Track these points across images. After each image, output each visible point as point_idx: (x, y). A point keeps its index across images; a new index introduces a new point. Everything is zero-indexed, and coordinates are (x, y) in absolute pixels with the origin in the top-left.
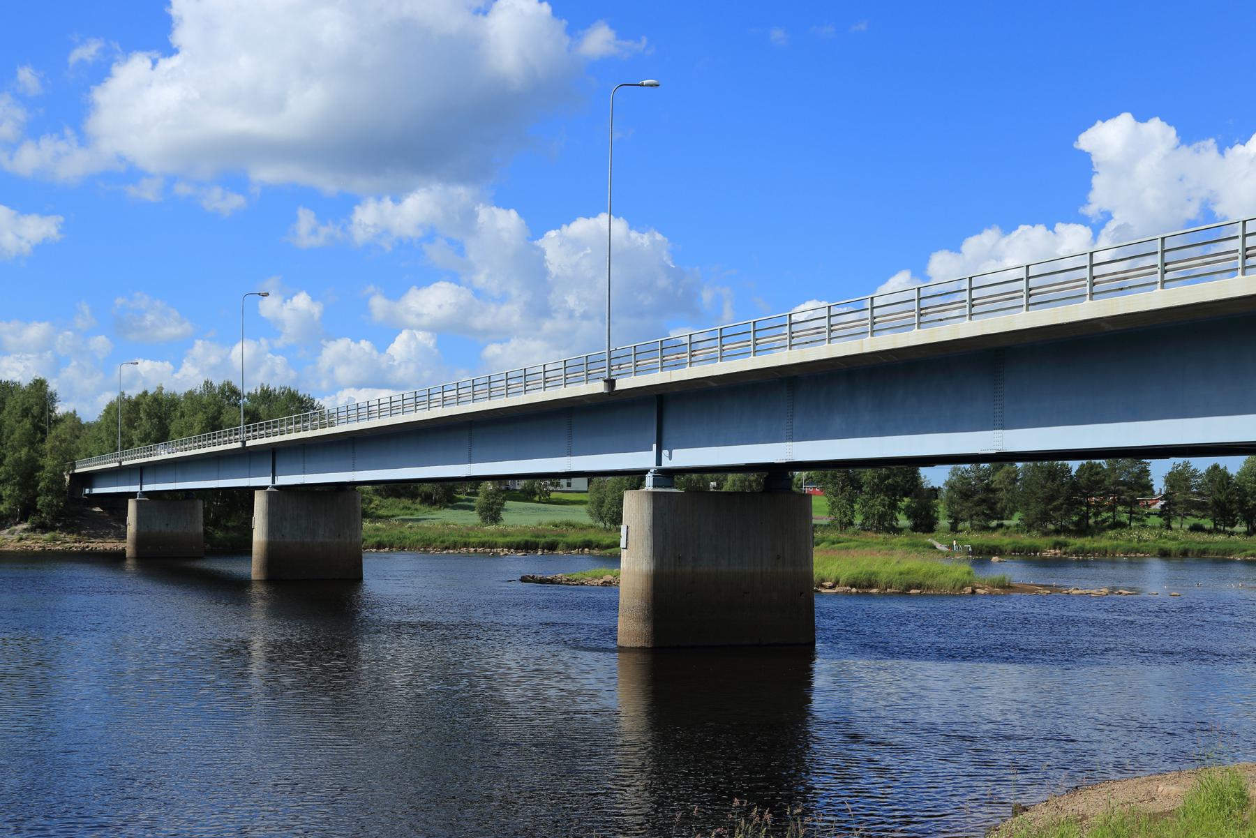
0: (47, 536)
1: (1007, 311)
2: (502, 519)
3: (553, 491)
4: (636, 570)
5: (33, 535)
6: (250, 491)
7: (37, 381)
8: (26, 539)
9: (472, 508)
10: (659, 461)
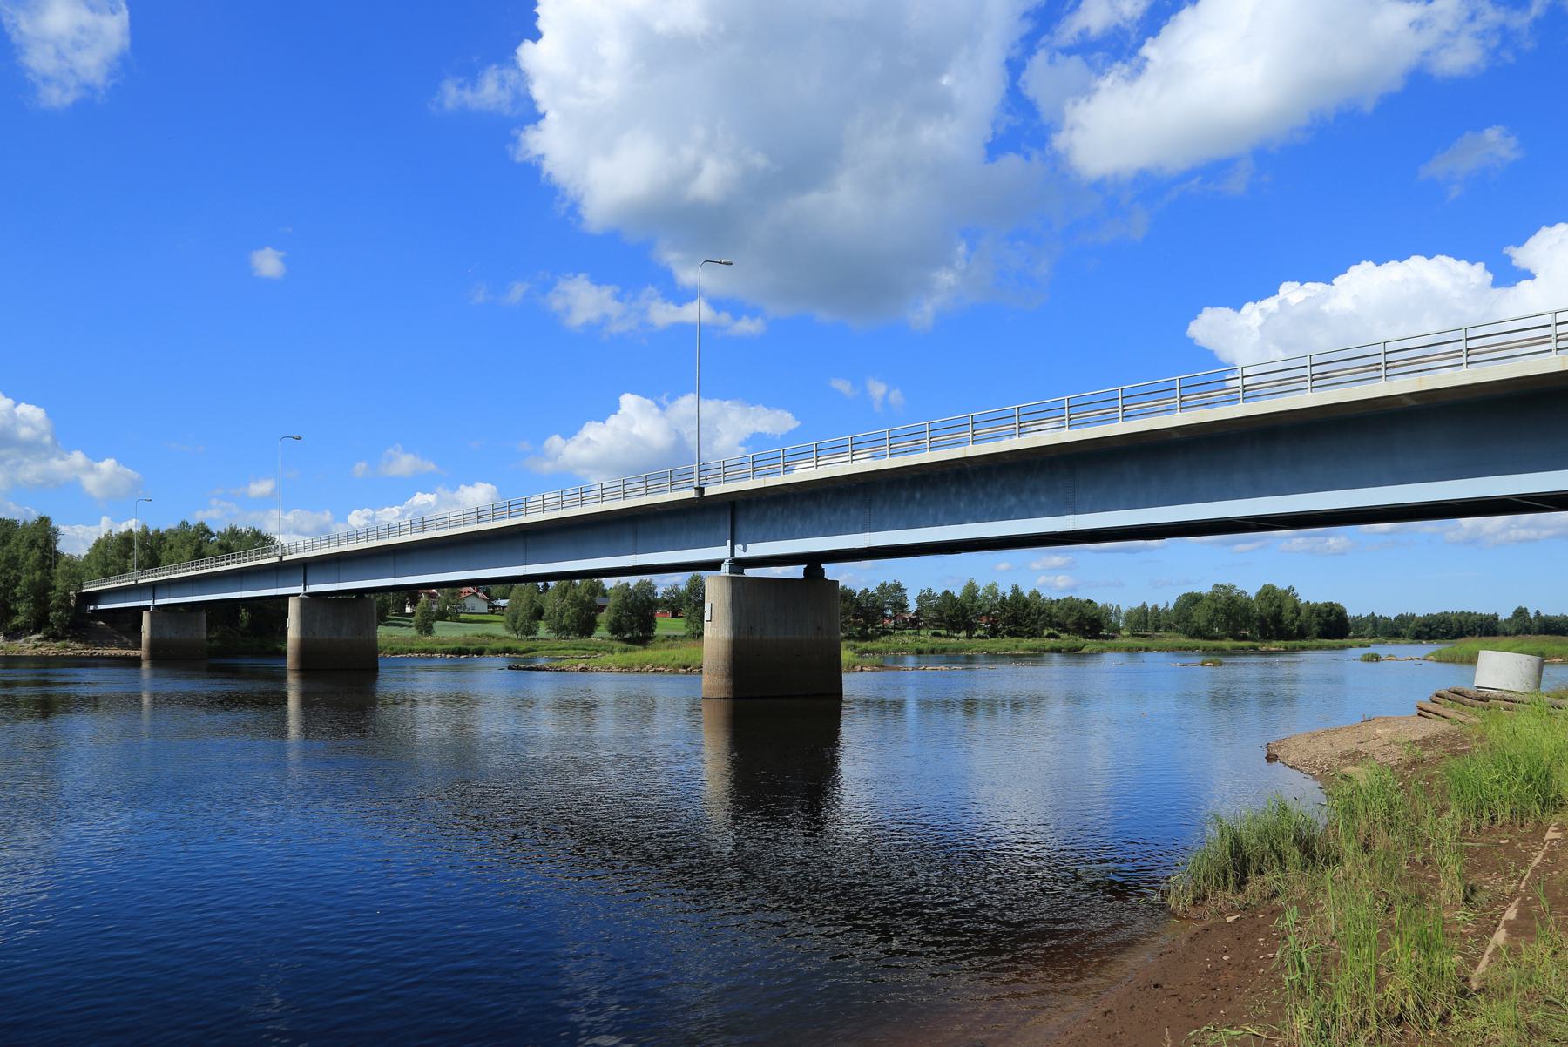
0: (59, 644)
1: (1495, 361)
2: (434, 632)
3: (461, 613)
5: (46, 643)
6: (287, 597)
7: (43, 518)
8: (41, 646)
9: (410, 626)
10: (732, 553)
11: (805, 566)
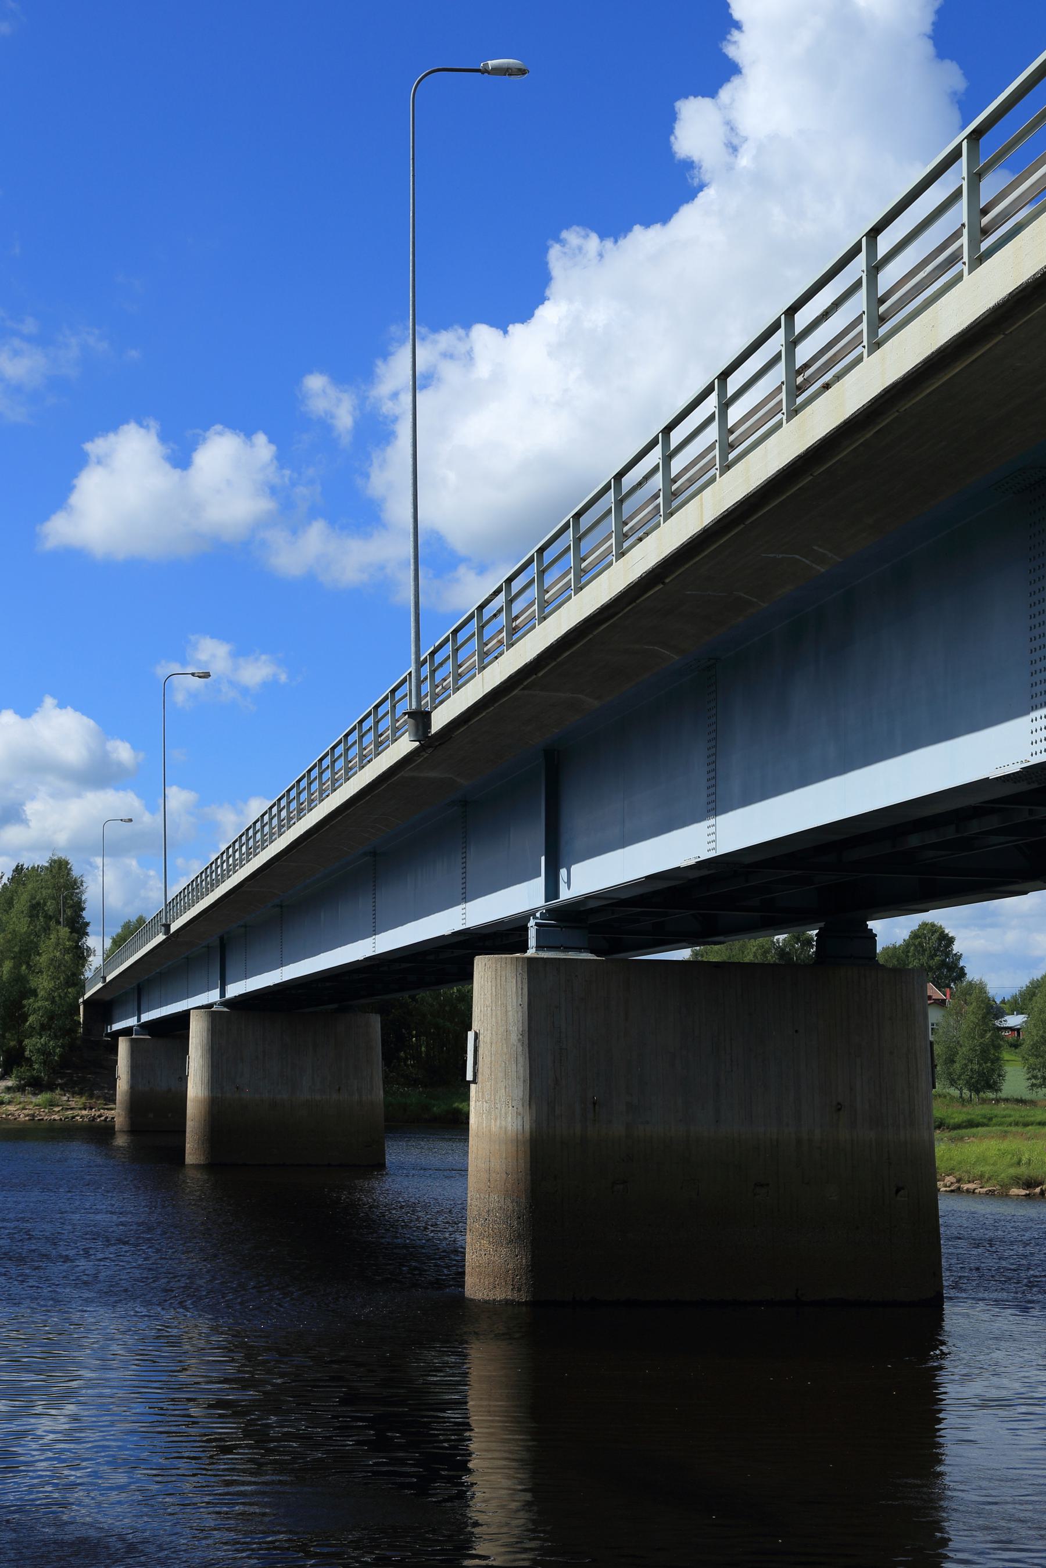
0: (40, 1098)
4: (493, 1129)
7: (55, 861)
8: (10, 1103)
11: (824, 923)
